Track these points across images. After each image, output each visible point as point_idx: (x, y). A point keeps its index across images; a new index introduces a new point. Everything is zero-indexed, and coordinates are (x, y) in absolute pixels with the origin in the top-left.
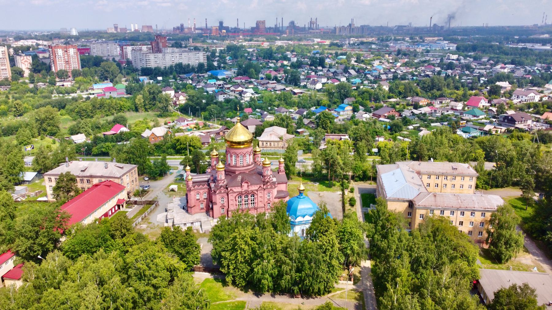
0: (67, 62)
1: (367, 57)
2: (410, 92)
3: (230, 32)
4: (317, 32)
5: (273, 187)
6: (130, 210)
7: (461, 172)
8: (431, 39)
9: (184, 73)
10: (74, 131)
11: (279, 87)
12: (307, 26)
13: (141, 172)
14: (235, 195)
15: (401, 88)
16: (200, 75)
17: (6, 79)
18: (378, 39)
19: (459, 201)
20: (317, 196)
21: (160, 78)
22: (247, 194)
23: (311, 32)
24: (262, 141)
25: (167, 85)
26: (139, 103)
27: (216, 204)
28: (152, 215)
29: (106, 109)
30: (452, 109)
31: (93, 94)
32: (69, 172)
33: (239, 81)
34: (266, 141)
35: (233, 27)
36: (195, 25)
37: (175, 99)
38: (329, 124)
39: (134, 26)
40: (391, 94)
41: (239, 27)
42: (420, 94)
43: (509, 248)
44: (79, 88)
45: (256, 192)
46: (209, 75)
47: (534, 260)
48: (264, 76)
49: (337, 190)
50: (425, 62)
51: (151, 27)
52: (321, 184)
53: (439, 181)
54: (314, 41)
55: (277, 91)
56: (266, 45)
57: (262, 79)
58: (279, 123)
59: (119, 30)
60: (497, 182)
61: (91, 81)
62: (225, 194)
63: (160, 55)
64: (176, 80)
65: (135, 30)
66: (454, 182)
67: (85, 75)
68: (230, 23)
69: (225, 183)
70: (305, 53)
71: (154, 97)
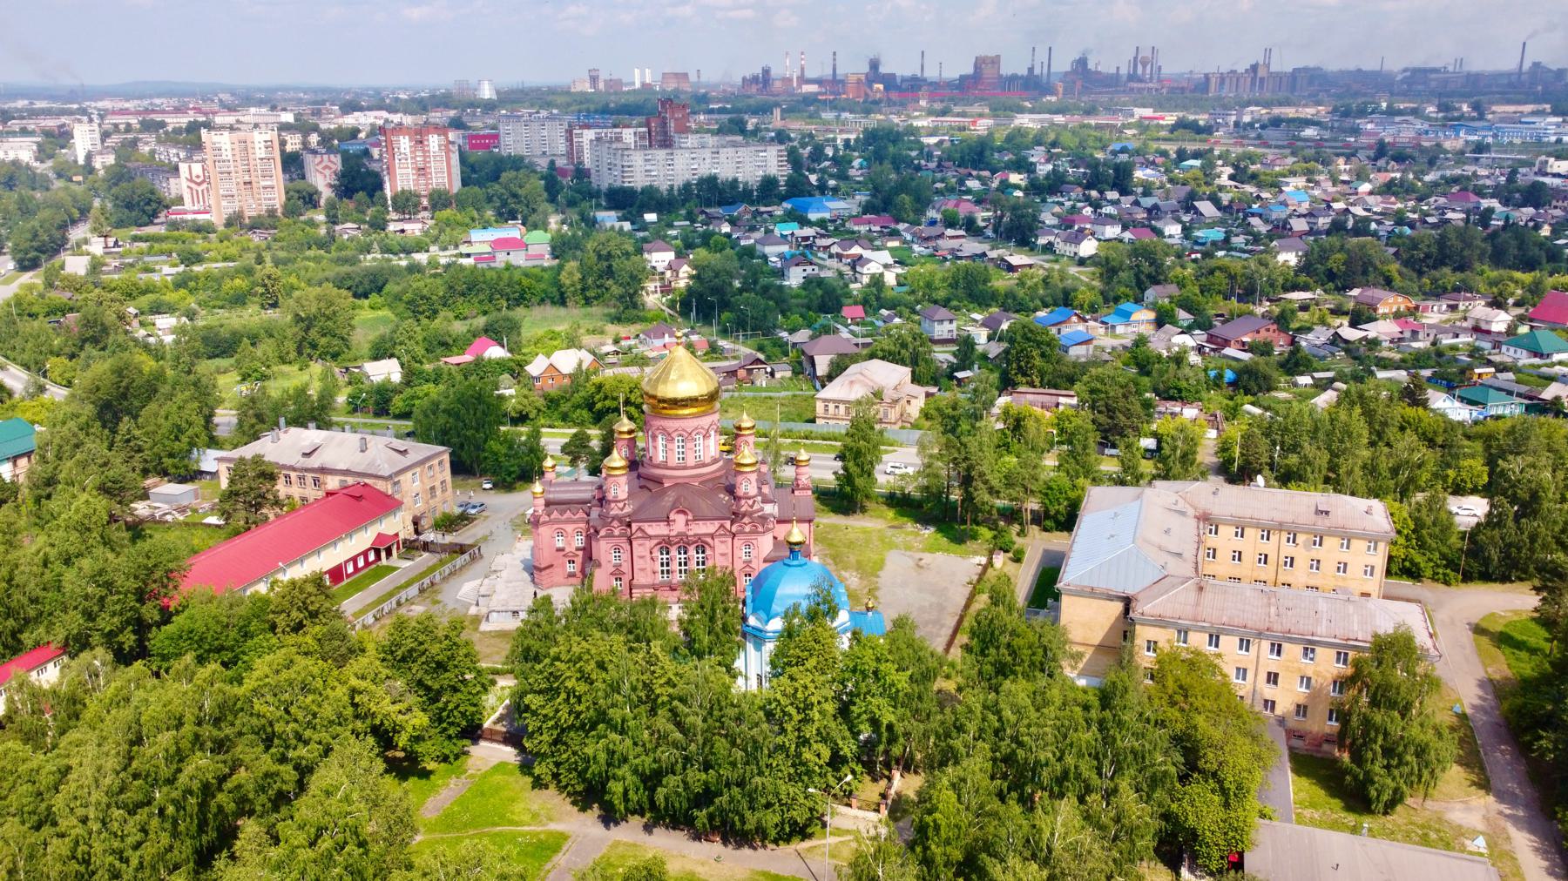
0: (422, 171)
1: (1273, 164)
2: (1365, 273)
3: (898, 88)
4: (1150, 89)
5: (760, 529)
6: (408, 564)
7: (1340, 522)
8: (1511, 108)
9: (720, 204)
10: (380, 352)
11: (972, 246)
12: (1124, 71)
13: (461, 468)
14: (650, 544)
15: (1336, 261)
16: (763, 209)
17: (272, 213)
18: (1335, 110)
19: (1273, 610)
20: (911, 563)
21: (651, 217)
22: (683, 544)
23: (1132, 89)
24: (825, 400)
25: (658, 237)
26: (568, 282)
27: (599, 565)
28: (453, 581)
29: (482, 297)
30: (1476, 329)
31: (468, 255)
32: (258, 456)
33: (863, 229)
34: (834, 401)
35: (908, 73)
36: (802, 69)
37: (668, 274)
38: (1038, 361)
39: (643, 74)
40: (1303, 278)
41: (927, 74)
42: (1398, 281)
43: (1397, 767)
44: (435, 240)
45: (709, 540)
46: (785, 210)
47: (1493, 814)
48: (939, 217)
49: (975, 553)
50: (1455, 180)
51: (685, 75)
52: (939, 530)
53: (1269, 547)
54: (1132, 115)
55: (960, 258)
56: (982, 126)
57: (933, 223)
58: (890, 353)
59: (601, 86)
60: (1487, 561)
61: (473, 220)
62: (624, 540)
63: (661, 154)
64: (693, 221)
65: (643, 84)
66: (1317, 552)
67: (460, 202)
68: (899, 65)
69: (628, 510)
70: (1088, 151)
71: (610, 267)
